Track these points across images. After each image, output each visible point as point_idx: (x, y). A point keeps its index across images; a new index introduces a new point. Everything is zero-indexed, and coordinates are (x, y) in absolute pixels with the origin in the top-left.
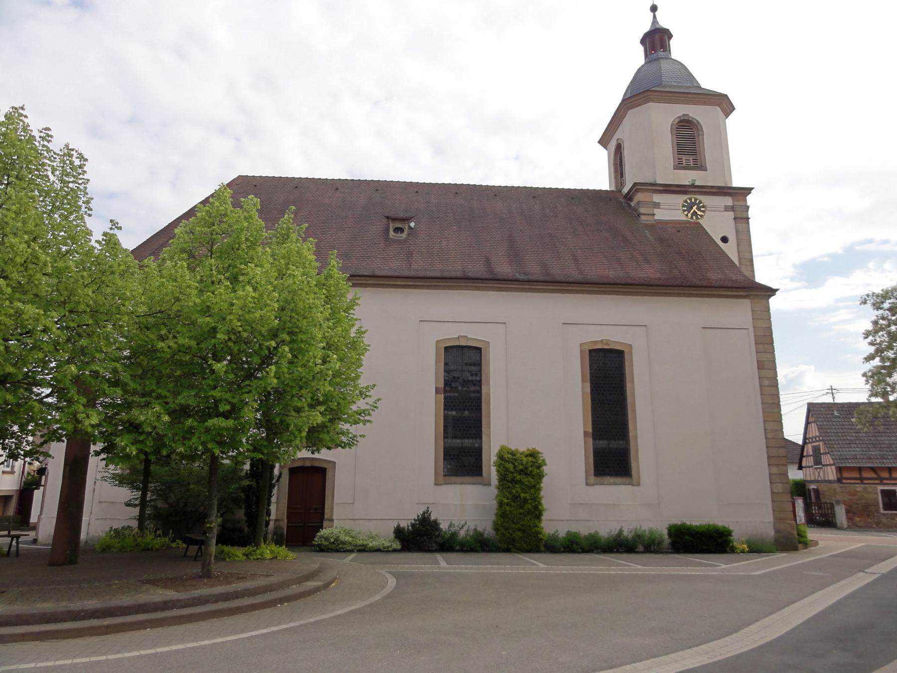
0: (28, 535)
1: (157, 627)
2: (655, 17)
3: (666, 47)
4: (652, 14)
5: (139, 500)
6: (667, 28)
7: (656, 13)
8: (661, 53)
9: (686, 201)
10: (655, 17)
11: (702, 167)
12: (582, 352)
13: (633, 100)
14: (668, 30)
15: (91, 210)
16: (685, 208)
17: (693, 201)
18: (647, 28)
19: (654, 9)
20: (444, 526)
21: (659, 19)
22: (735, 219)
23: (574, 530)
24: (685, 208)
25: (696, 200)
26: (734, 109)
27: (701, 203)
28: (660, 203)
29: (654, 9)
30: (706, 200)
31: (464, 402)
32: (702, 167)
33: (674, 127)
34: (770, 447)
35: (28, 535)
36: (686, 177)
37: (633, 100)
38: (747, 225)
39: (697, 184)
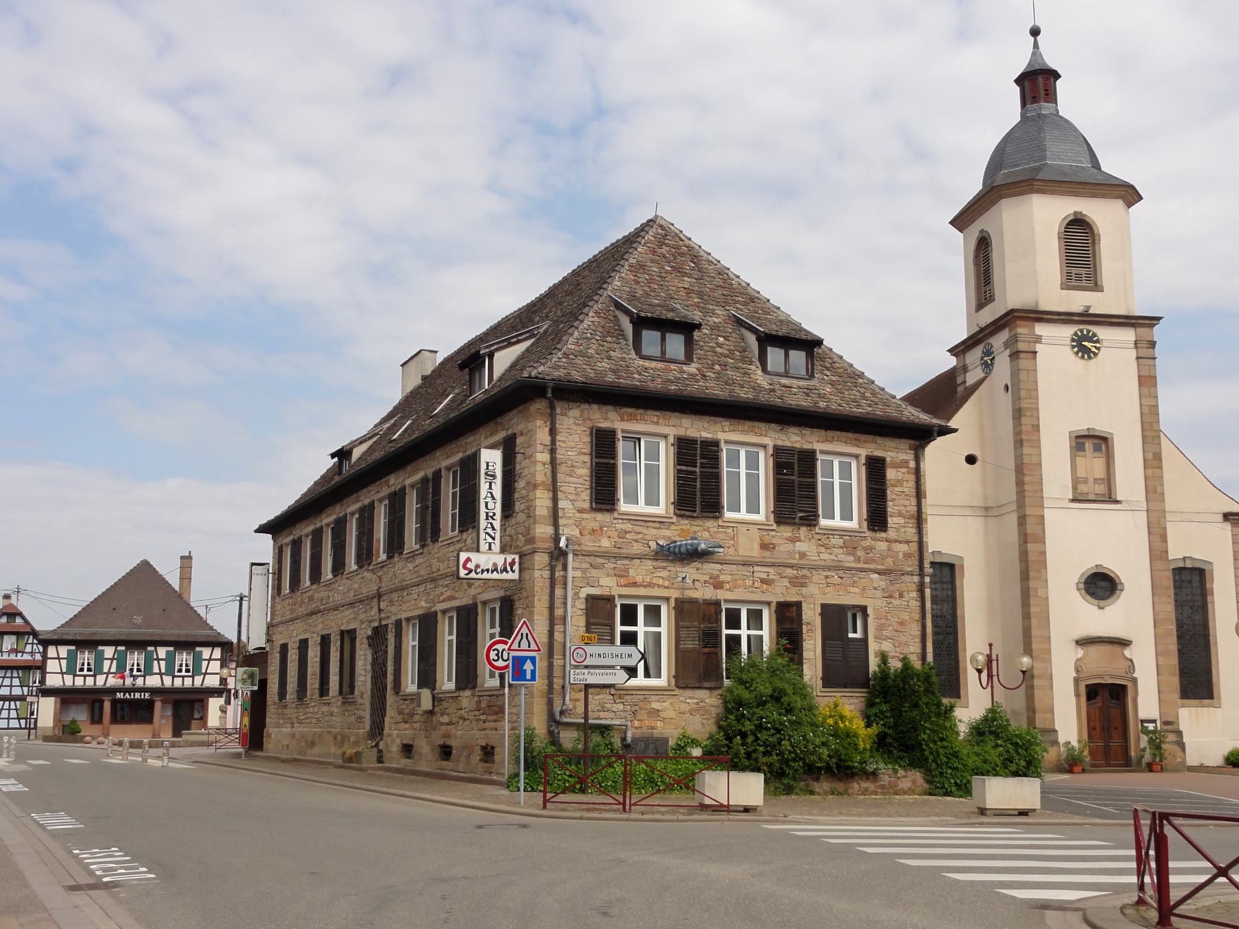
0: (997, 655)
1: (678, 333)
2: (1036, 45)
3: (1051, 96)
6: (1055, 69)
8: (1046, 108)
9: (1081, 331)
10: (1036, 45)
11: (1096, 287)
14: (1056, 71)
15: (492, 573)
17: (1085, 333)
19: (1035, 32)
20: (954, 714)
21: (1042, 49)
22: (1138, 358)
23: (1234, 746)
24: (1075, 344)
25: (1089, 331)
27: (1096, 336)
28: (1041, 336)
30: (1102, 332)
32: (1096, 287)
35: (997, 655)
36: (1078, 301)
38: (1141, 374)
39: (1091, 311)
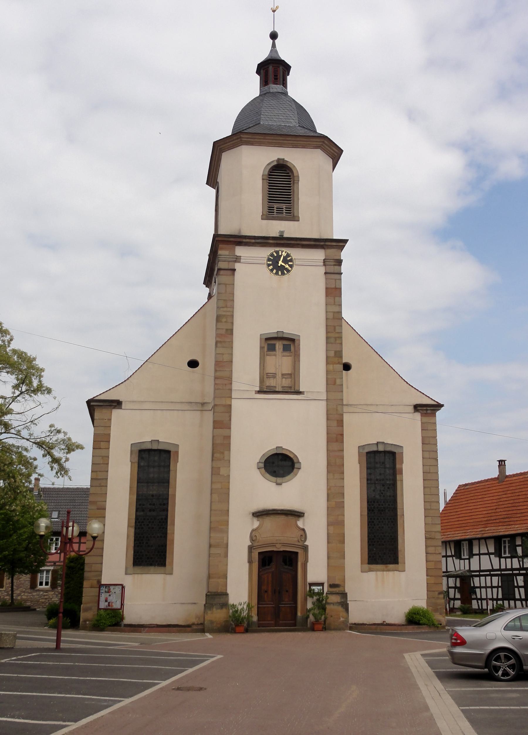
2: (274, 45)
4: (272, 41)
5: (71, 516)
7: (276, 41)
10: (274, 45)
11: (295, 218)
12: (261, 339)
13: (213, 164)
16: (271, 263)
18: (263, 55)
19: (274, 36)
21: (278, 48)
22: (325, 273)
24: (271, 263)
26: (342, 151)
29: (274, 36)
30: (296, 254)
31: (385, 542)
32: (295, 218)
33: (265, 177)
34: (100, 556)
37: (213, 164)
39: (285, 235)
